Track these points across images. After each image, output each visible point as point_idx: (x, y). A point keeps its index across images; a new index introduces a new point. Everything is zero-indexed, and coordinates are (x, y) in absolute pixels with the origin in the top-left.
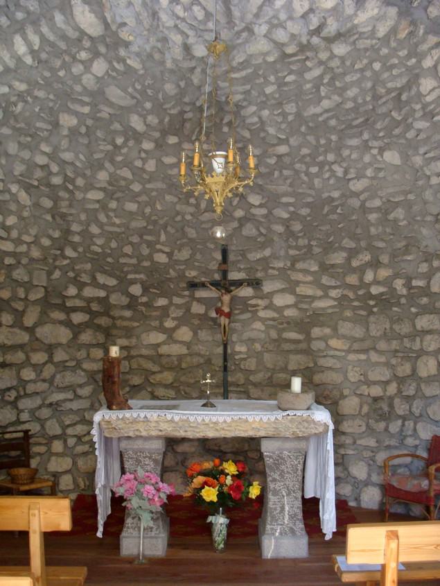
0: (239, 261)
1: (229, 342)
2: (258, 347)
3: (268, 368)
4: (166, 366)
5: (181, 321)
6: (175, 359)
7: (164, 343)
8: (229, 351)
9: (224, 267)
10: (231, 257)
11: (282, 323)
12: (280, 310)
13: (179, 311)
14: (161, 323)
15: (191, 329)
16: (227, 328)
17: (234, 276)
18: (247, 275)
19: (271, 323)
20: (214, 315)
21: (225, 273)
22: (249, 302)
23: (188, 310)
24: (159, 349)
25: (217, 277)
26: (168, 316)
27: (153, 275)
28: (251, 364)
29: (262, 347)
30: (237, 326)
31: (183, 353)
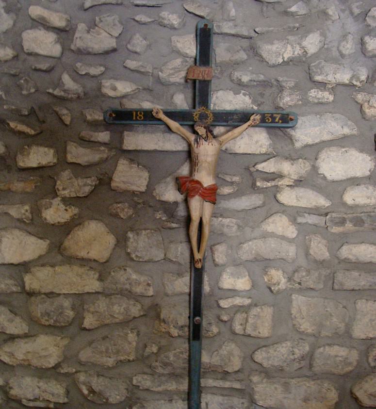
0: (237, 64)
1: (208, 265)
2: (278, 277)
3: (302, 333)
4: (43, 322)
5: (88, 206)
6: (67, 303)
7: (40, 261)
8: (206, 288)
9: (201, 73)
10: (220, 51)
11: (342, 222)
12: (334, 189)
13: (81, 182)
14: (36, 212)
15: (112, 230)
16: (206, 230)
17: (224, 100)
18: (254, 102)
19: (312, 219)
20: (171, 194)
21: (200, 91)
22: (260, 167)
23: (105, 181)
24: (27, 279)
25: (181, 101)
26: (54, 194)
27: (20, 87)
28: (262, 322)
29: (290, 279)
30: (229, 224)
31: (87, 289)
